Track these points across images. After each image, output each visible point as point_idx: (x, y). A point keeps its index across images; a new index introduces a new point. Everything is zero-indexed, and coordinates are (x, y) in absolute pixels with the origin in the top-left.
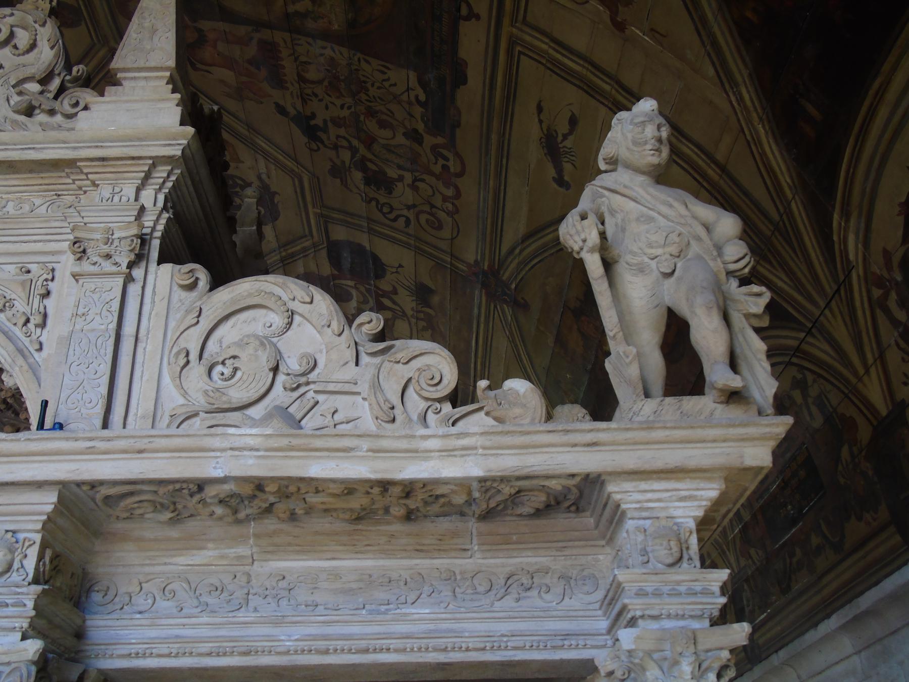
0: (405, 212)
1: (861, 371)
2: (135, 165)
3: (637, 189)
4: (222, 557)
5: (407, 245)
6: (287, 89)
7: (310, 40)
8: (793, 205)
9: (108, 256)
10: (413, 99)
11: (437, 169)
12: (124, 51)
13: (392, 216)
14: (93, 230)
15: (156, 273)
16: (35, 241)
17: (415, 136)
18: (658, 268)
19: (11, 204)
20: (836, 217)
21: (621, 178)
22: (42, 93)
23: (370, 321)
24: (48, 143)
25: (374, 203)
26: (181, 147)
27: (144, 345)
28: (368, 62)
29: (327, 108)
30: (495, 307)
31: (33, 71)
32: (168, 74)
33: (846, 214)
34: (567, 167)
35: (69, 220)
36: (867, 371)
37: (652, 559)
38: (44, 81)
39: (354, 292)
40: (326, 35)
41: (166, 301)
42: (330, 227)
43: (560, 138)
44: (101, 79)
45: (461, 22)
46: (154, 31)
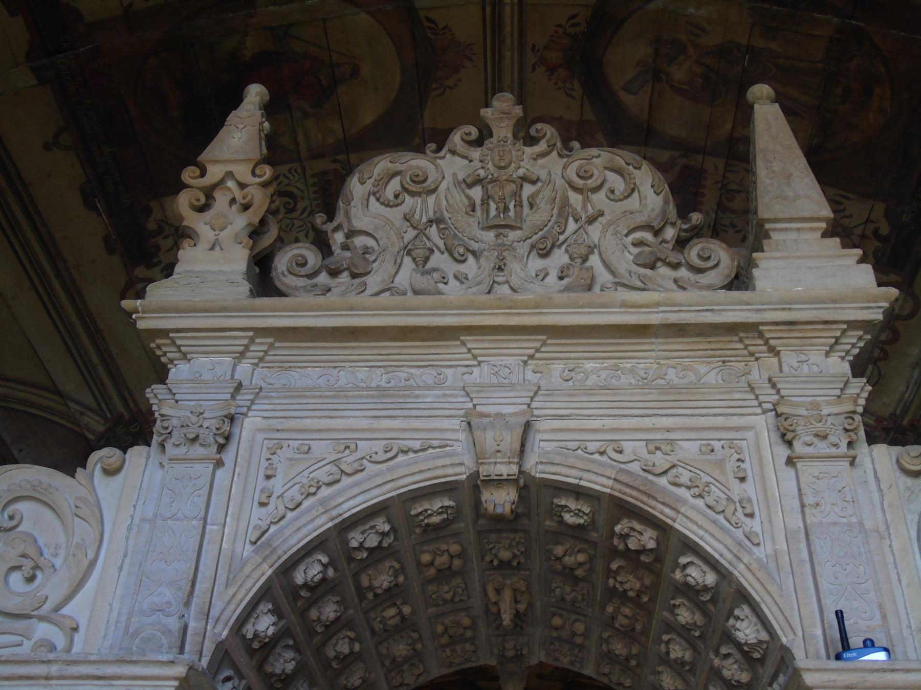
2: (826, 329)
10: (869, 232)
15: (871, 456)
16: (715, 415)
26: (882, 310)
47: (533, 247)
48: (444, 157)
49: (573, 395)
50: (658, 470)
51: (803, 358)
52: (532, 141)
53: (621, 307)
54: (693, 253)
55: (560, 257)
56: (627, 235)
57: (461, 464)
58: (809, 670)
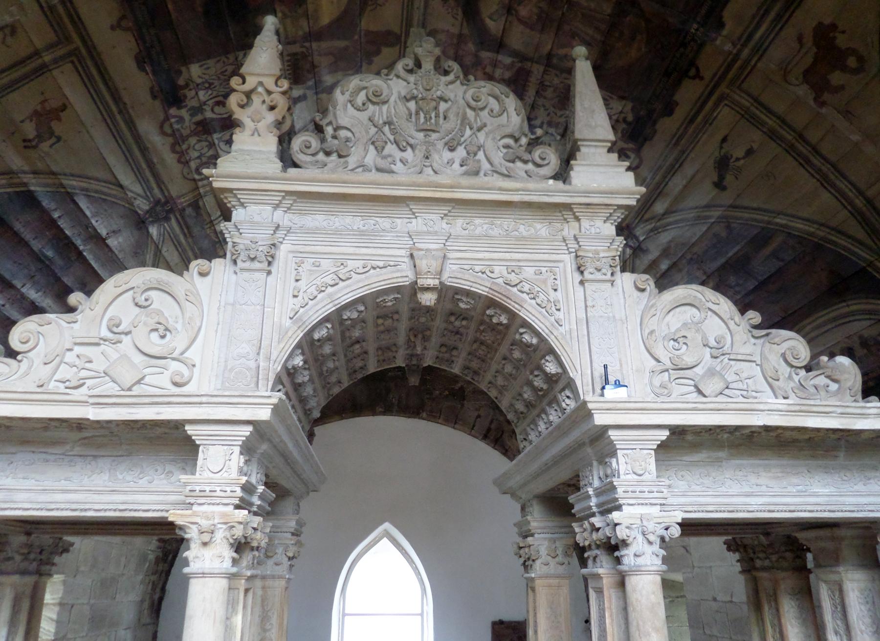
4: (708, 458)
7: (558, 73)
23: (754, 316)
29: (548, 115)
32: (609, 144)
52: (446, 73)
55: (461, 152)
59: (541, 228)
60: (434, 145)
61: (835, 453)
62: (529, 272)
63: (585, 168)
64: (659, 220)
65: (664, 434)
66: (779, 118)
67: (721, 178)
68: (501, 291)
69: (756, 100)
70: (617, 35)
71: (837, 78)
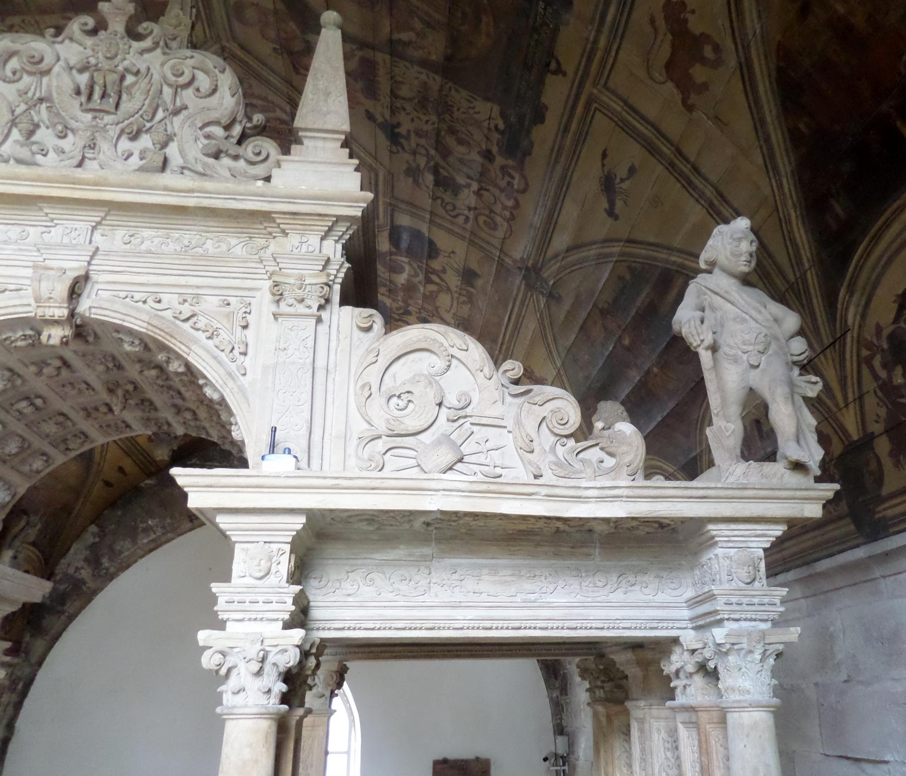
0: (466, 212)
1: (842, 405)
3: (733, 293)
4: (410, 555)
5: (463, 238)
6: (379, 100)
8: (809, 273)
9: (302, 301)
10: (492, 126)
11: (503, 184)
12: (304, 110)
13: (453, 214)
14: (287, 276)
16: (234, 278)
17: (488, 156)
18: (748, 361)
19: (209, 242)
20: (843, 291)
21: (719, 281)
22: (226, 138)
24: (248, 195)
25: (439, 201)
27: (333, 376)
28: (457, 90)
29: (412, 120)
30: (532, 295)
31: (217, 115)
32: (343, 137)
33: (851, 291)
34: (619, 204)
35: (265, 263)
36: (847, 406)
37: (735, 578)
38: (228, 128)
39: (407, 267)
40: (424, 63)
41: (349, 339)
42: (396, 214)
43: (618, 180)
44: (286, 137)
45: (549, 75)
46: (328, 94)
47: (122, 131)
48: (62, 42)
49: (124, 256)
50: (183, 317)
51: (304, 239)
52: (138, 37)
53: (164, 190)
54: (249, 149)
55: (145, 141)
56: (201, 128)
57: (29, 305)
58: (180, 475)
59: (234, 243)
60: (104, 129)
61: (585, 550)
62: (211, 303)
63: (297, 165)
64: (563, 259)
65: (778, 531)
66: (653, 125)
67: (612, 203)
68: (163, 327)
69: (625, 102)
70: (459, 14)
71: (699, 73)
